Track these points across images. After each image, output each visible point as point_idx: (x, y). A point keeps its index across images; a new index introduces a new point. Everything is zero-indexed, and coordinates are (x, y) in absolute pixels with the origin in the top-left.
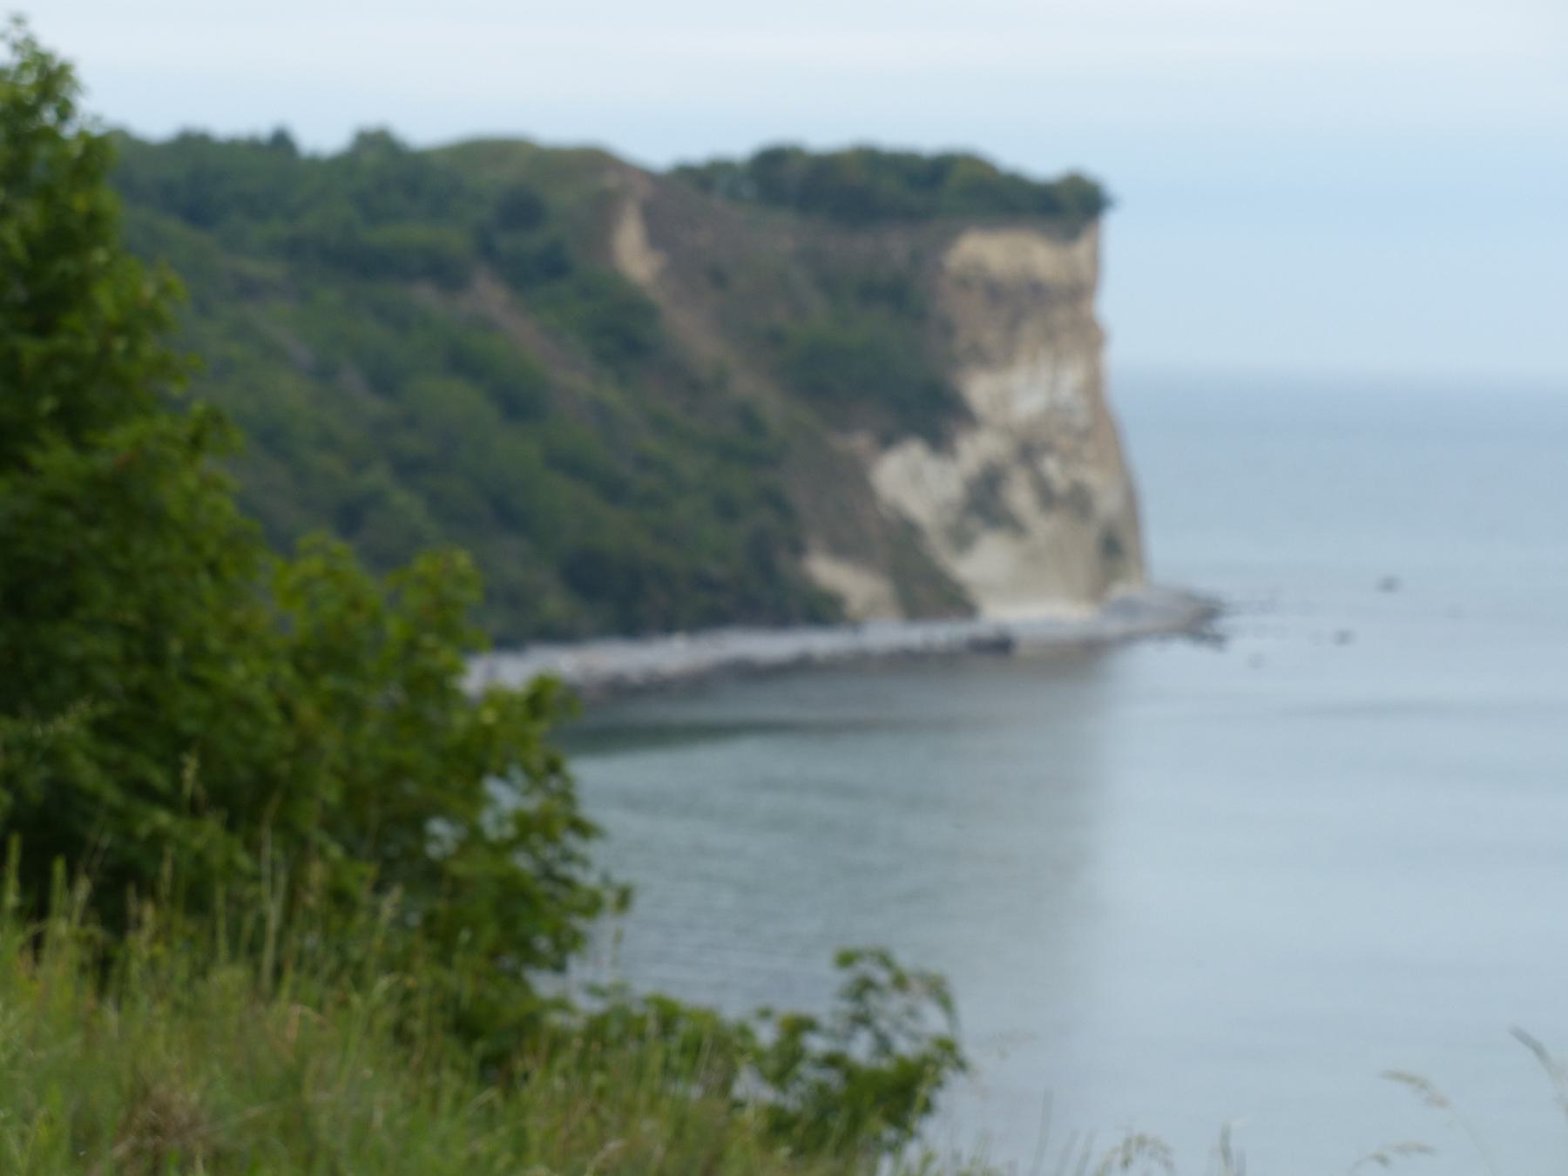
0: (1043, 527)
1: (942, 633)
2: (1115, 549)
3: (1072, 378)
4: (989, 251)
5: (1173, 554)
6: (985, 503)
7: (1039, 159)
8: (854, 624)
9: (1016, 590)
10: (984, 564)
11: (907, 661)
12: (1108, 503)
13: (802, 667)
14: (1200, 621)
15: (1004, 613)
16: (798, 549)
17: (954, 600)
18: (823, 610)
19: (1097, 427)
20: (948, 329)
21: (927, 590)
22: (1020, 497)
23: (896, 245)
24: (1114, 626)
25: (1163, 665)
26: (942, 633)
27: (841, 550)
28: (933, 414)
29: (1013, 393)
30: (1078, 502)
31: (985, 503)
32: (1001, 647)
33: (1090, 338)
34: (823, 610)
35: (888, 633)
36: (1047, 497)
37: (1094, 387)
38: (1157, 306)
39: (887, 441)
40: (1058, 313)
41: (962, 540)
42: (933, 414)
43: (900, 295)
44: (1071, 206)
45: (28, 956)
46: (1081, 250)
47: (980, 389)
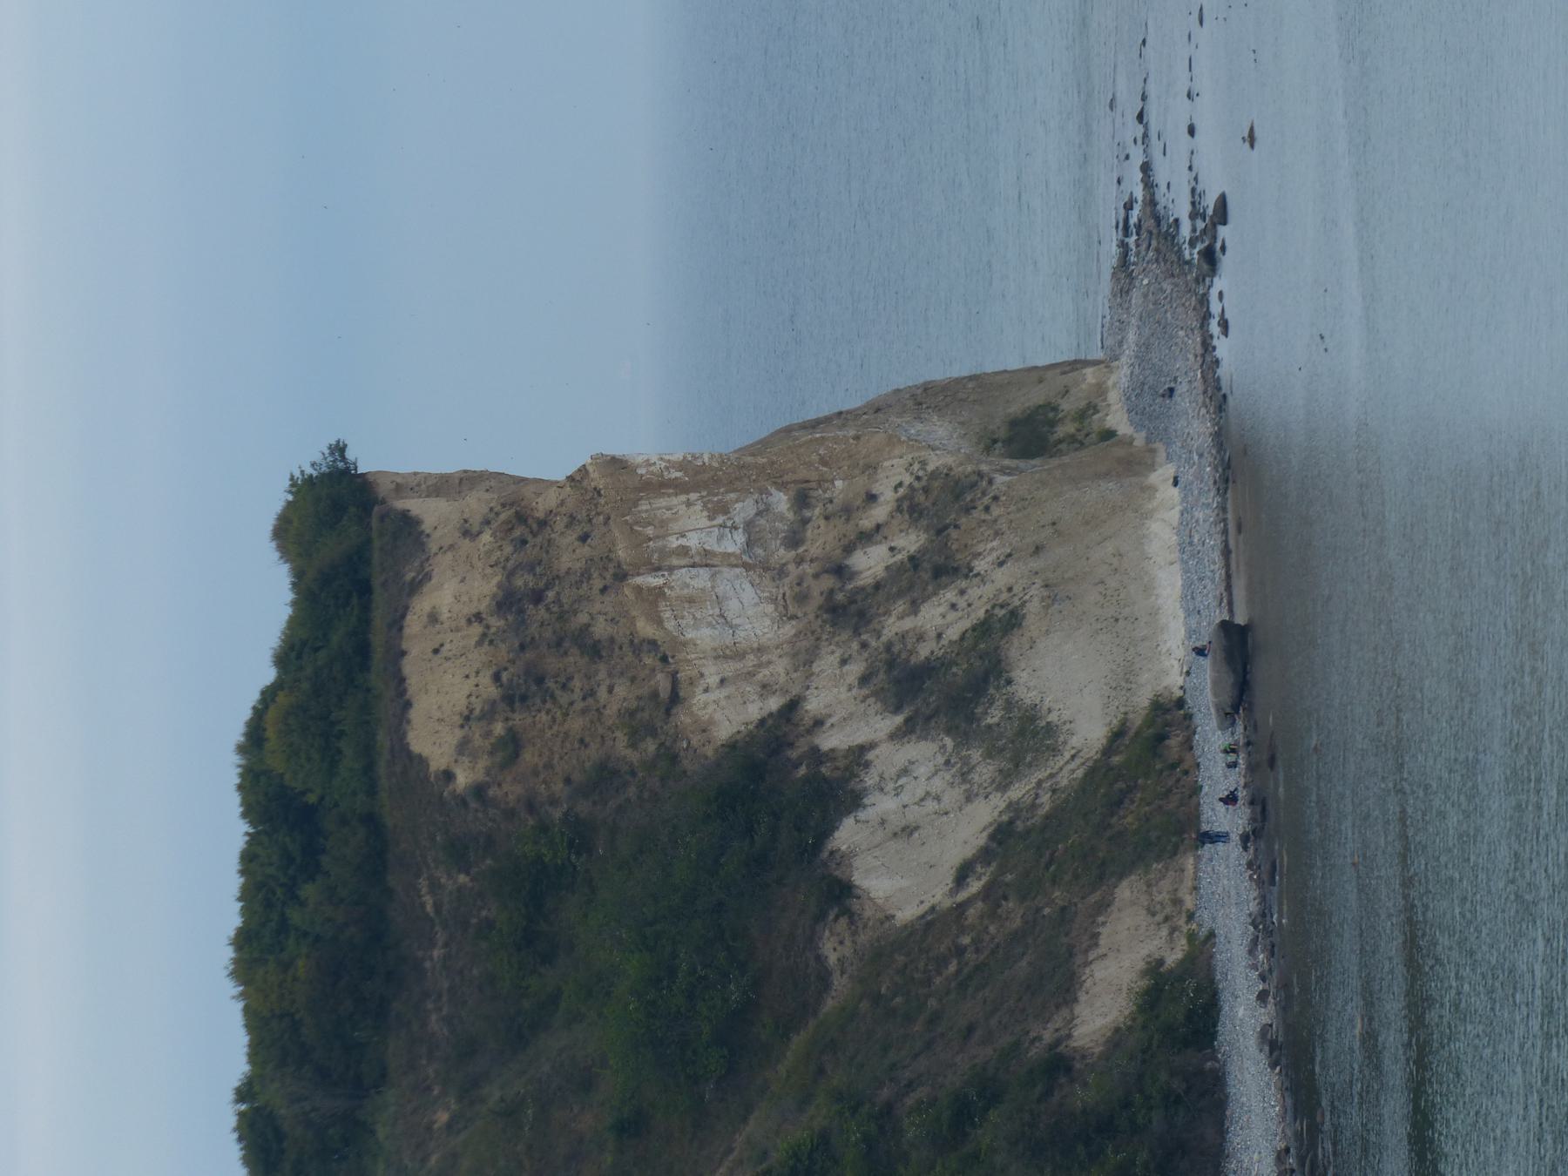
0: (994, 578)
1: (1217, 770)
2: (1036, 426)
3: (693, 527)
4: (442, 700)
5: (1041, 311)
6: (953, 694)
7: (265, 598)
8: (1202, 948)
9: (1117, 637)
10: (1075, 690)
11: (1281, 837)
12: (945, 444)
13: (1293, 1052)
14: (1173, 252)
15: (1173, 652)
16: (1059, 1064)
17: (1156, 736)
18: (1180, 1009)
19: (792, 474)
20: (606, 776)
21: (1130, 803)
22: (940, 621)
23: (435, 889)
24: (1193, 424)
25: (1280, 328)
26: (1217, 770)
27: (1060, 984)
28: (779, 799)
29: (728, 642)
30: (942, 503)
31: (953, 694)
32: (1236, 647)
33: (611, 488)
34: (1180, 1009)
35: (1224, 888)
36: (939, 568)
37: (705, 480)
38: (541, 361)
39: (839, 894)
40: (562, 555)
41: (1032, 735)
42: (779, 799)
43: (538, 874)
44: (345, 535)
45: (1247, 144)
46: (431, 512)
47: (723, 712)
